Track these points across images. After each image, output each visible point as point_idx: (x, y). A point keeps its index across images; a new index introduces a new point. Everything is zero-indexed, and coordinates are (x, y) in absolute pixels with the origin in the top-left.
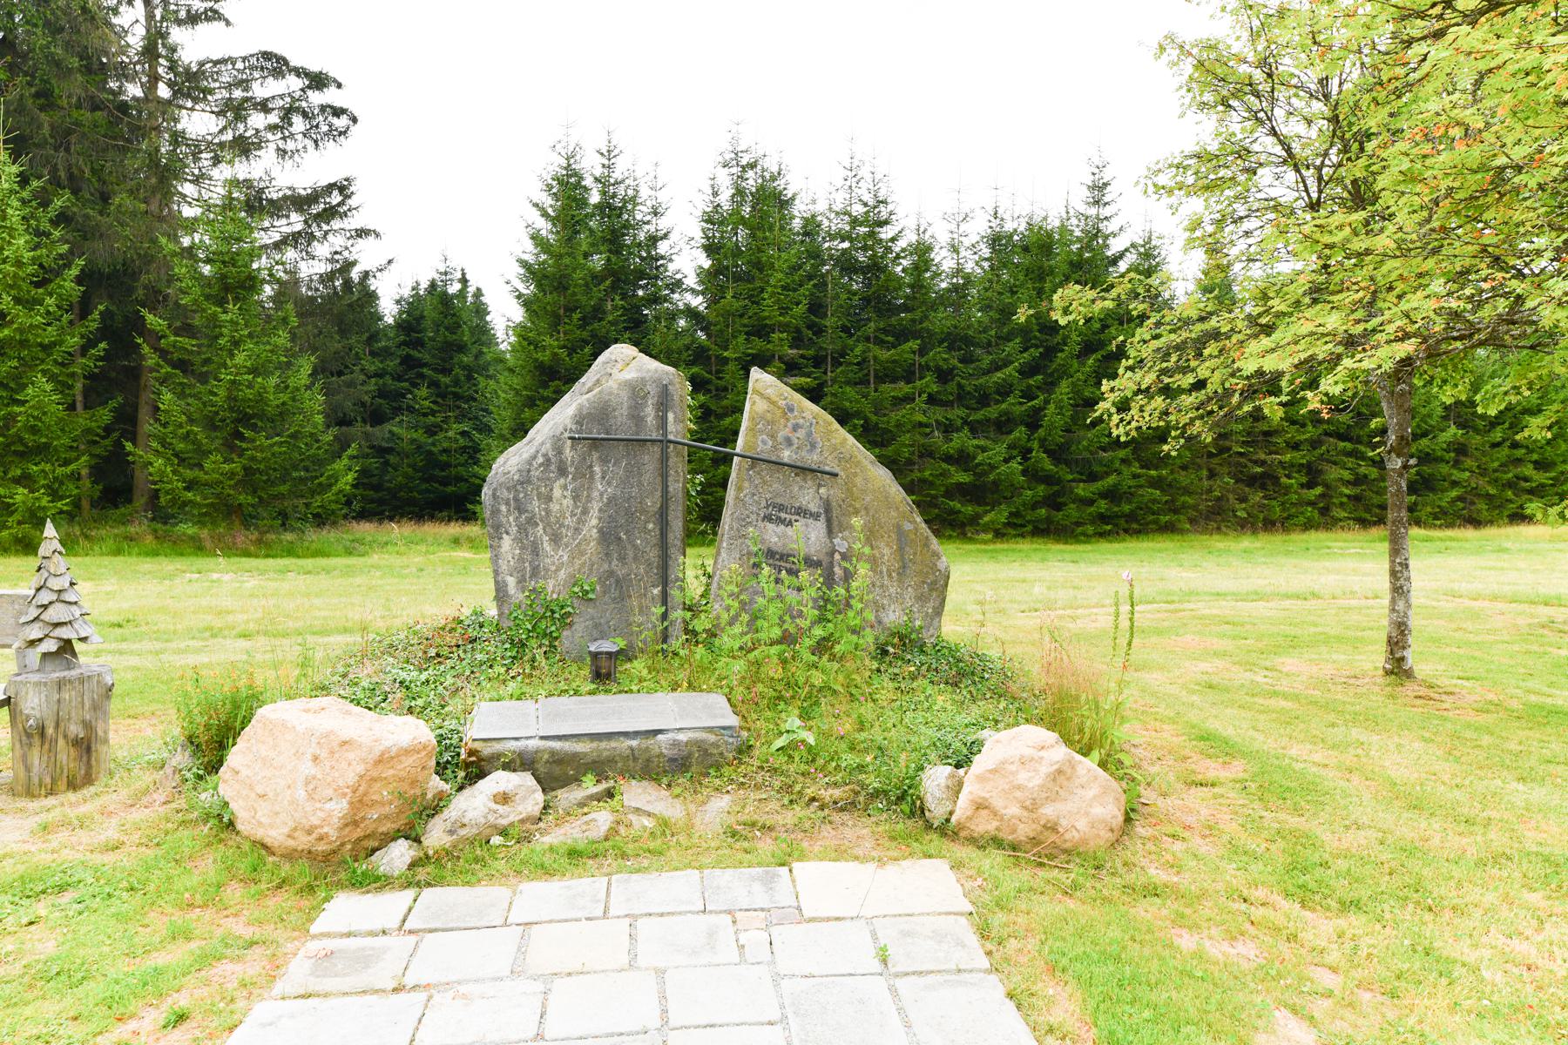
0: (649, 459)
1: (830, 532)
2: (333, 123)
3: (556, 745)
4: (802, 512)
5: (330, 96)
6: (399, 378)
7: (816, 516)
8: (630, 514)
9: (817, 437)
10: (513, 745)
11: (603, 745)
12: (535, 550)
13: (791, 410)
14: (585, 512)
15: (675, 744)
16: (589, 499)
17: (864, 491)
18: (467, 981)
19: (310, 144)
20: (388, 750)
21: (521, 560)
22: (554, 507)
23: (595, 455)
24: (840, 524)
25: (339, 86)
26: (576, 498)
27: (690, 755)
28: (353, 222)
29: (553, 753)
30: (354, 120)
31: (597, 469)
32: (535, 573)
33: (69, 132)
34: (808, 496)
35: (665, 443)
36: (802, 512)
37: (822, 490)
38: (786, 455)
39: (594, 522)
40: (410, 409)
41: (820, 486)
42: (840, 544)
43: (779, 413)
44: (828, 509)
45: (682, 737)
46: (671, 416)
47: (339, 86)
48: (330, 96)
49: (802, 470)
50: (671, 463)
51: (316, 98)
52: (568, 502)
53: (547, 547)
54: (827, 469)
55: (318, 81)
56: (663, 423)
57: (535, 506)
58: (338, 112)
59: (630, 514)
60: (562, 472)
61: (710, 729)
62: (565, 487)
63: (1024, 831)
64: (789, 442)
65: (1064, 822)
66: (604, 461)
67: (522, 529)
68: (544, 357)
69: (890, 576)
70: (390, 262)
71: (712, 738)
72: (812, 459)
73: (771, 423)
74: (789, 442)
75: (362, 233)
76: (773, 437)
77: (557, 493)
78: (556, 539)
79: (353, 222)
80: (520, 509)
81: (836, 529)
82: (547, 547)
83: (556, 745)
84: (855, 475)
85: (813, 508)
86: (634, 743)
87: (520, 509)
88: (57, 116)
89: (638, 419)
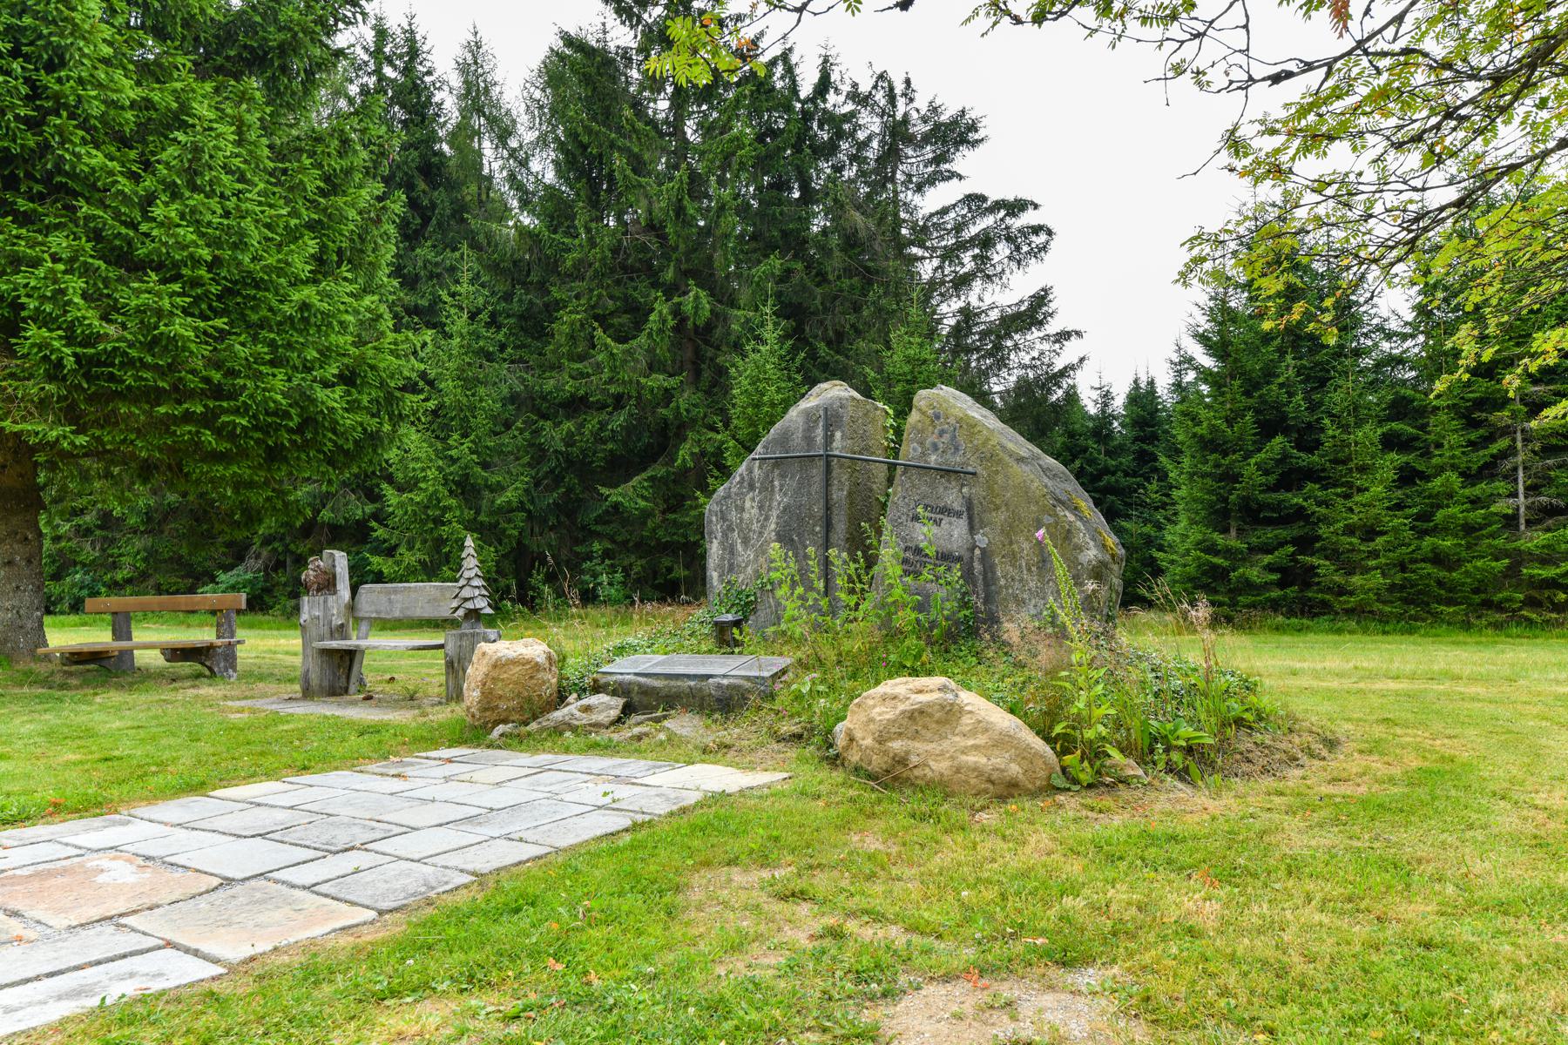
0: (817, 472)
1: (972, 529)
2: (1030, 243)
3: (642, 680)
4: (946, 511)
5: (1028, 218)
6: (1135, 475)
7: (958, 515)
8: (800, 519)
9: (961, 440)
10: (614, 678)
11: (673, 683)
12: (732, 551)
13: (938, 417)
14: (767, 518)
15: (719, 686)
16: (770, 508)
17: (1005, 488)
18: (188, 677)
19: (1014, 265)
20: (499, 659)
21: (723, 559)
22: (746, 516)
23: (777, 472)
24: (981, 521)
25: (1036, 207)
26: (761, 508)
27: (731, 698)
28: (1053, 327)
29: (640, 685)
30: (1050, 233)
31: (776, 483)
32: (731, 569)
33: (836, 297)
34: (952, 497)
35: (828, 459)
36: (946, 511)
37: (965, 490)
38: (933, 459)
39: (773, 526)
40: (1143, 504)
41: (963, 485)
42: (982, 540)
43: (928, 421)
44: (970, 508)
45: (725, 682)
46: (838, 435)
47: (1036, 207)
48: (1028, 218)
49: (946, 473)
50: (834, 474)
51: (1017, 223)
52: (755, 511)
53: (740, 547)
54: (970, 469)
55: (1017, 207)
56: (829, 439)
57: (733, 516)
58: (1037, 230)
59: (800, 519)
60: (752, 487)
61: (748, 678)
62: (753, 499)
63: (877, 763)
64: (935, 447)
65: (914, 760)
66: (783, 476)
67: (725, 535)
68: (1202, 430)
69: (1029, 570)
70: (1082, 360)
71: (748, 685)
72: (955, 461)
73: (921, 431)
74: (935, 447)
75: (1064, 336)
76: (921, 444)
77: (748, 504)
78: (746, 541)
79: (1053, 327)
80: (724, 519)
81: (977, 526)
82: (740, 547)
83: (642, 680)
84: (997, 472)
85: (957, 506)
86: (692, 683)
87: (724, 519)
88: (826, 288)
89: (809, 440)
